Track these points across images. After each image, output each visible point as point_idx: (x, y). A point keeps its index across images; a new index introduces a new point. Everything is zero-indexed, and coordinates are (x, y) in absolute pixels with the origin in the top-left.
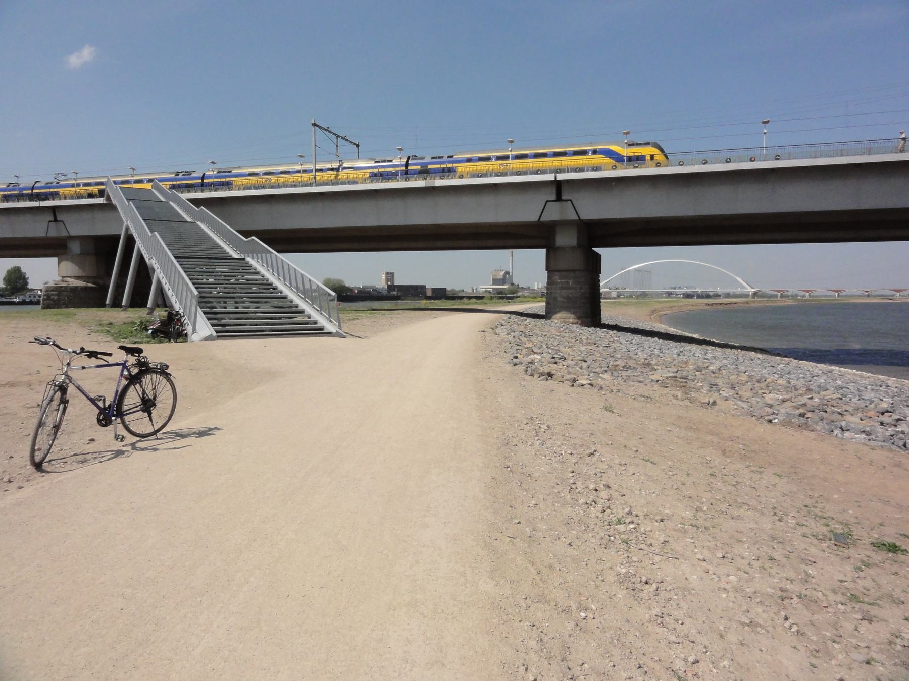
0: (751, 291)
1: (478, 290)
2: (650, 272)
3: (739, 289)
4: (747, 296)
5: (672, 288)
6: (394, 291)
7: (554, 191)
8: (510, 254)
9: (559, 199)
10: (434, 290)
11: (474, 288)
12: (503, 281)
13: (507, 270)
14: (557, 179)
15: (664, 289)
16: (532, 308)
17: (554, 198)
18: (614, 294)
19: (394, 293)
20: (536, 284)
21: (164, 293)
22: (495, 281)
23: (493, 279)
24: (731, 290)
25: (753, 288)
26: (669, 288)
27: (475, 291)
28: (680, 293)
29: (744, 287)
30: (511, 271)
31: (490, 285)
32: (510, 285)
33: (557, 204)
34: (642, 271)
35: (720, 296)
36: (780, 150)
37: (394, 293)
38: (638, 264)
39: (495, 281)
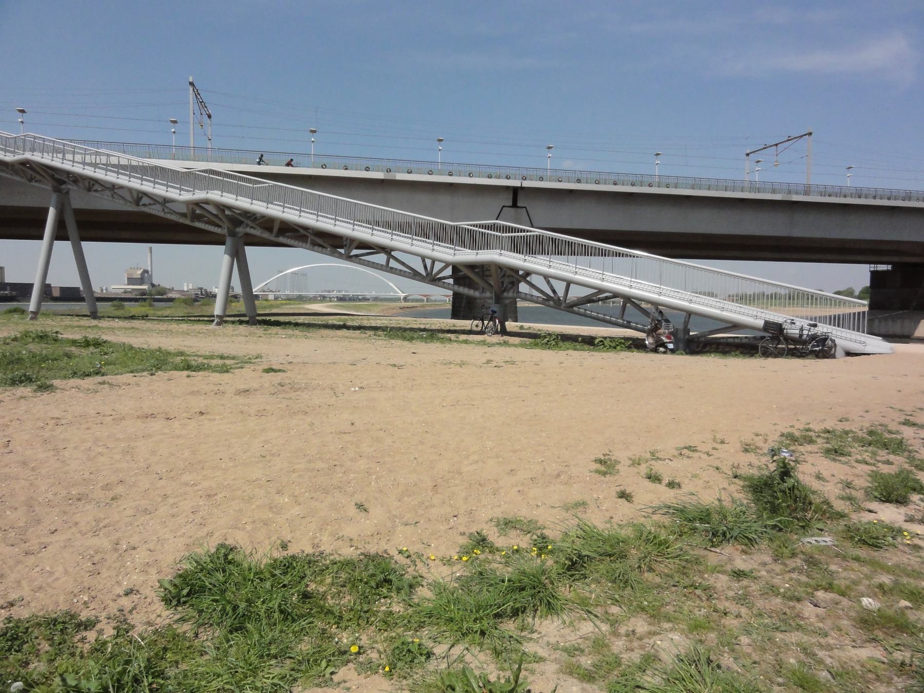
0: (402, 295)
1: (109, 290)
2: (306, 275)
3: (392, 294)
4: (398, 299)
5: (326, 291)
6: (5, 290)
7: (511, 196)
8: (148, 250)
9: (515, 205)
10: (63, 290)
11: (104, 288)
12: (141, 281)
13: (146, 268)
14: (523, 186)
15: (317, 292)
16: (548, 327)
17: (511, 204)
18: (271, 297)
19: (6, 292)
20: (185, 284)
21: (611, 325)
22: (131, 281)
23: (128, 278)
24: (382, 294)
25: (403, 293)
26: (322, 292)
27: (104, 291)
28: (335, 296)
29: (395, 292)
30: (149, 269)
31: (125, 285)
32: (150, 285)
33: (512, 210)
34: (297, 274)
35: (369, 299)
36: (508, 170)
37: (6, 292)
38: (296, 267)
39: (131, 281)
